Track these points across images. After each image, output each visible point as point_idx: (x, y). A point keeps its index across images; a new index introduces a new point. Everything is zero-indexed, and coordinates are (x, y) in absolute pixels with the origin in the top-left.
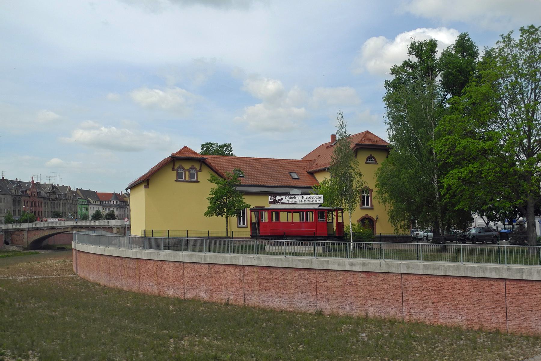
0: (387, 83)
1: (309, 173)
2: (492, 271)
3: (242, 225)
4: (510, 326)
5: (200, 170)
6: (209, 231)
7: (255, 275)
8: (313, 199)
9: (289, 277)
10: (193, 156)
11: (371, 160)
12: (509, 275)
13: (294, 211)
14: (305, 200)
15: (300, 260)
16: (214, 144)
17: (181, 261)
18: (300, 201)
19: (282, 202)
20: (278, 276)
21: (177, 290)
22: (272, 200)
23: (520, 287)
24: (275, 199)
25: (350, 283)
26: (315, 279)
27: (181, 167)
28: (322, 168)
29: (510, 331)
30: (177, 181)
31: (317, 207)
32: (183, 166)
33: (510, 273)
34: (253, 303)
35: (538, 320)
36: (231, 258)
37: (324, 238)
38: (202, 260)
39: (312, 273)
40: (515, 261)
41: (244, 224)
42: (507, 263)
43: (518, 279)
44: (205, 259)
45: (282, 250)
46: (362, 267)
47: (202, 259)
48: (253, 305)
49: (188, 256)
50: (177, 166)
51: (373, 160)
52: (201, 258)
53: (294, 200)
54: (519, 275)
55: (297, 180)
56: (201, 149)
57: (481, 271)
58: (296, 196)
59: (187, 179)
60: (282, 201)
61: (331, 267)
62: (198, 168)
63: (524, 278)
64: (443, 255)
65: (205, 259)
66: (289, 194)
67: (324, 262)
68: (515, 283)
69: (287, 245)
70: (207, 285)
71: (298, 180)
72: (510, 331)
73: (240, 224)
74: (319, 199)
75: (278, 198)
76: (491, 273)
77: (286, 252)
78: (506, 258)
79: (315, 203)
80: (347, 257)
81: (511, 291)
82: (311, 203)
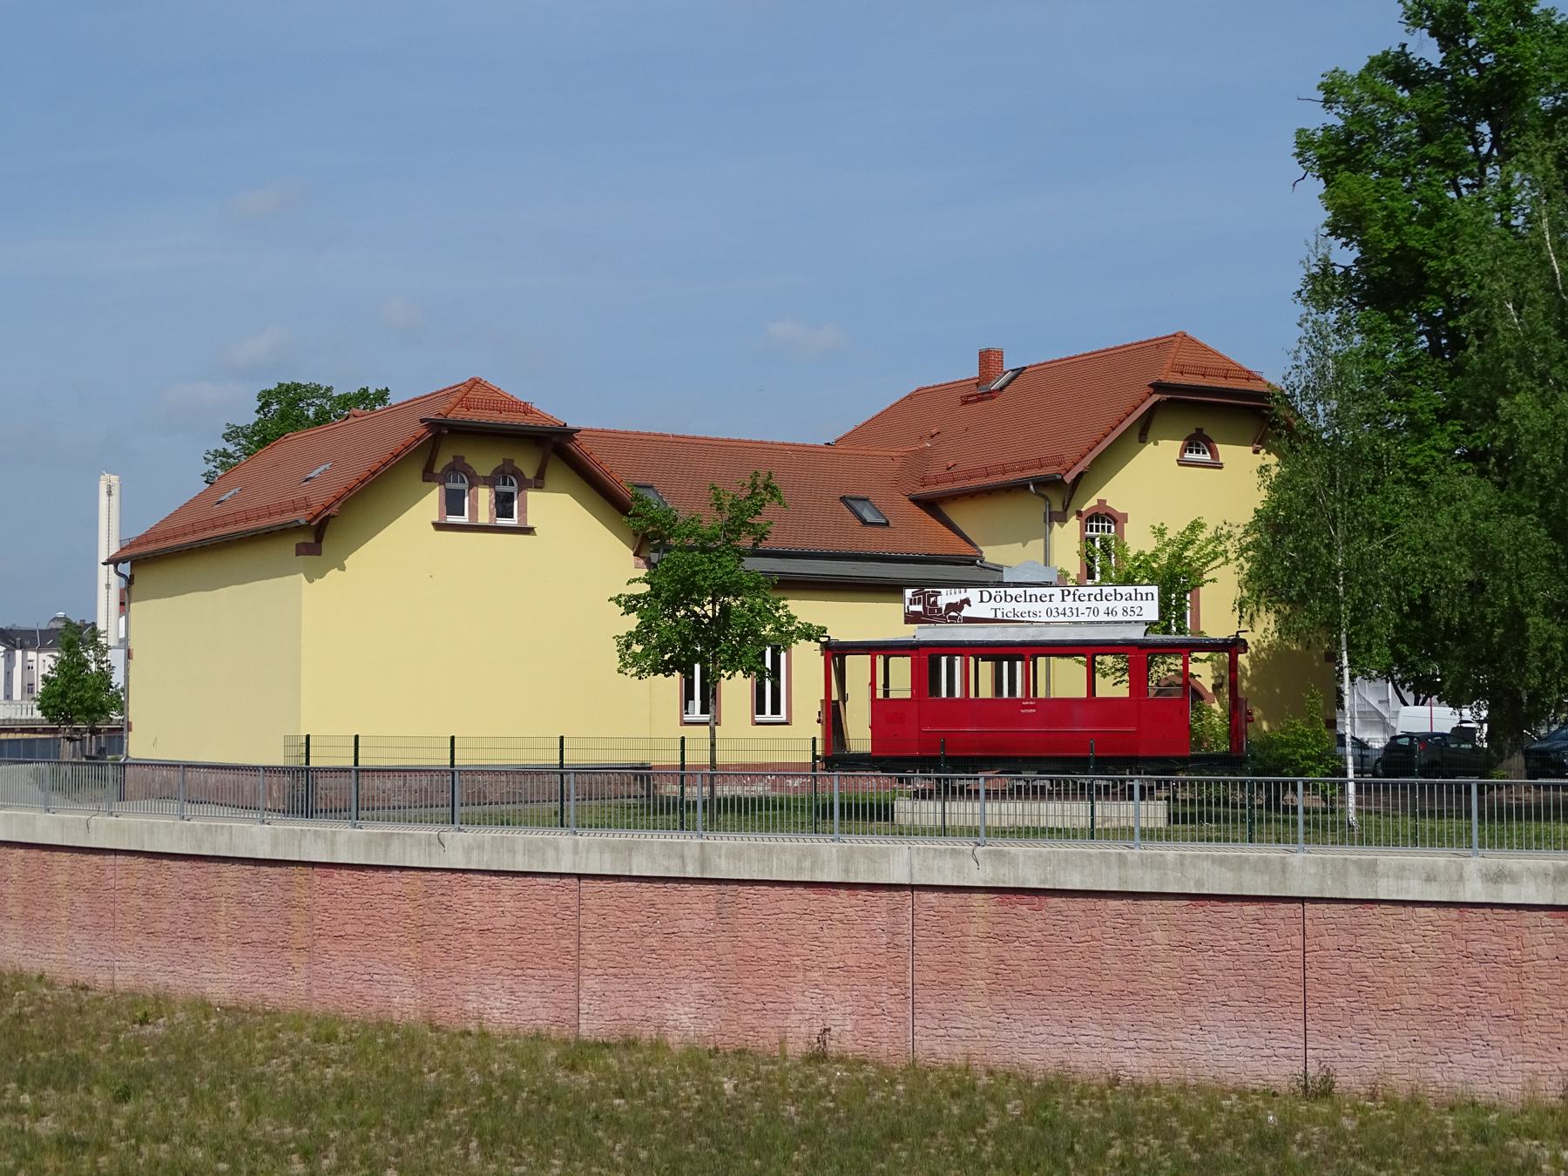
0: (1304, 143)
1: (917, 501)
3: (768, 716)
5: (539, 483)
6: (357, 737)
7: (977, 928)
8: (1111, 605)
9: (1158, 935)
10: (519, 419)
11: (1198, 452)
13: (982, 651)
14: (1074, 605)
15: (1222, 861)
16: (315, 391)
17: (565, 868)
18: (1049, 612)
19: (963, 614)
20: (1096, 932)
21: (534, 1000)
22: (919, 608)
24: (935, 603)
25: (1484, 958)
26: (1297, 940)
27: (458, 469)
28: (1011, 477)
30: (439, 526)
31: (1137, 634)
32: (516, 464)
34: (959, 1048)
35: (1418, 1044)
36: (847, 859)
37: (1165, 765)
38: (684, 865)
39: (1281, 914)
41: (704, 710)
42: (1480, 847)
44: (703, 862)
45: (969, 818)
46: (1550, 887)
47: (688, 860)
48: (959, 1061)
49: (614, 849)
50: (443, 461)
51: (512, 484)
52: (682, 857)
53: (1022, 607)
55: (879, 530)
56: (258, 412)
58: (1030, 591)
59: (484, 518)
60: (967, 612)
61: (1385, 889)
62: (529, 474)
65: (703, 862)
66: (1001, 584)
67: (1352, 869)
69: (992, 795)
70: (708, 974)
71: (886, 529)
73: (760, 709)
74: (1139, 603)
77: (988, 823)
79: (1120, 618)
80: (453, 823)
82: (1102, 617)
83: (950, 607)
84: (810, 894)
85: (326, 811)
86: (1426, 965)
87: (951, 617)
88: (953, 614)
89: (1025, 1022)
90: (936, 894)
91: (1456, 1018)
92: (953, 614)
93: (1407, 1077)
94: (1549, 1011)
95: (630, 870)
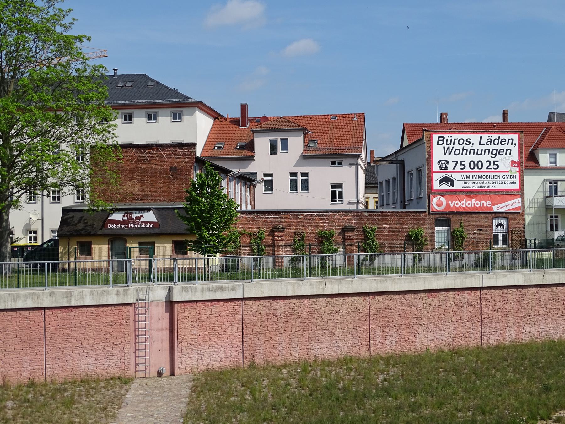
2: (27, 298)
4: (49, 372)
12: (52, 301)
23: (66, 316)
24: (132, 216)
29: (48, 379)
33: (54, 298)
40: (96, 281)
43: (64, 305)
54: (65, 300)
57: (10, 300)
60: (142, 220)
63: (73, 304)
64: (30, 278)
68: (59, 312)
72: (48, 379)
75: (135, 215)
76: (26, 301)
78: (305, 273)
81: (54, 323)
83: (137, 218)
84: (122, 307)
85: (318, 267)
86: (91, 328)
87: (137, 222)
88: (137, 220)
89: (11, 364)
90: (28, 312)
91: (101, 347)
92: (137, 220)
93: (17, 377)
94: (377, 324)
95: (263, 293)
